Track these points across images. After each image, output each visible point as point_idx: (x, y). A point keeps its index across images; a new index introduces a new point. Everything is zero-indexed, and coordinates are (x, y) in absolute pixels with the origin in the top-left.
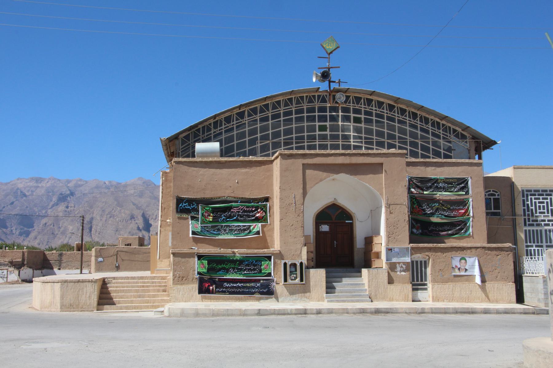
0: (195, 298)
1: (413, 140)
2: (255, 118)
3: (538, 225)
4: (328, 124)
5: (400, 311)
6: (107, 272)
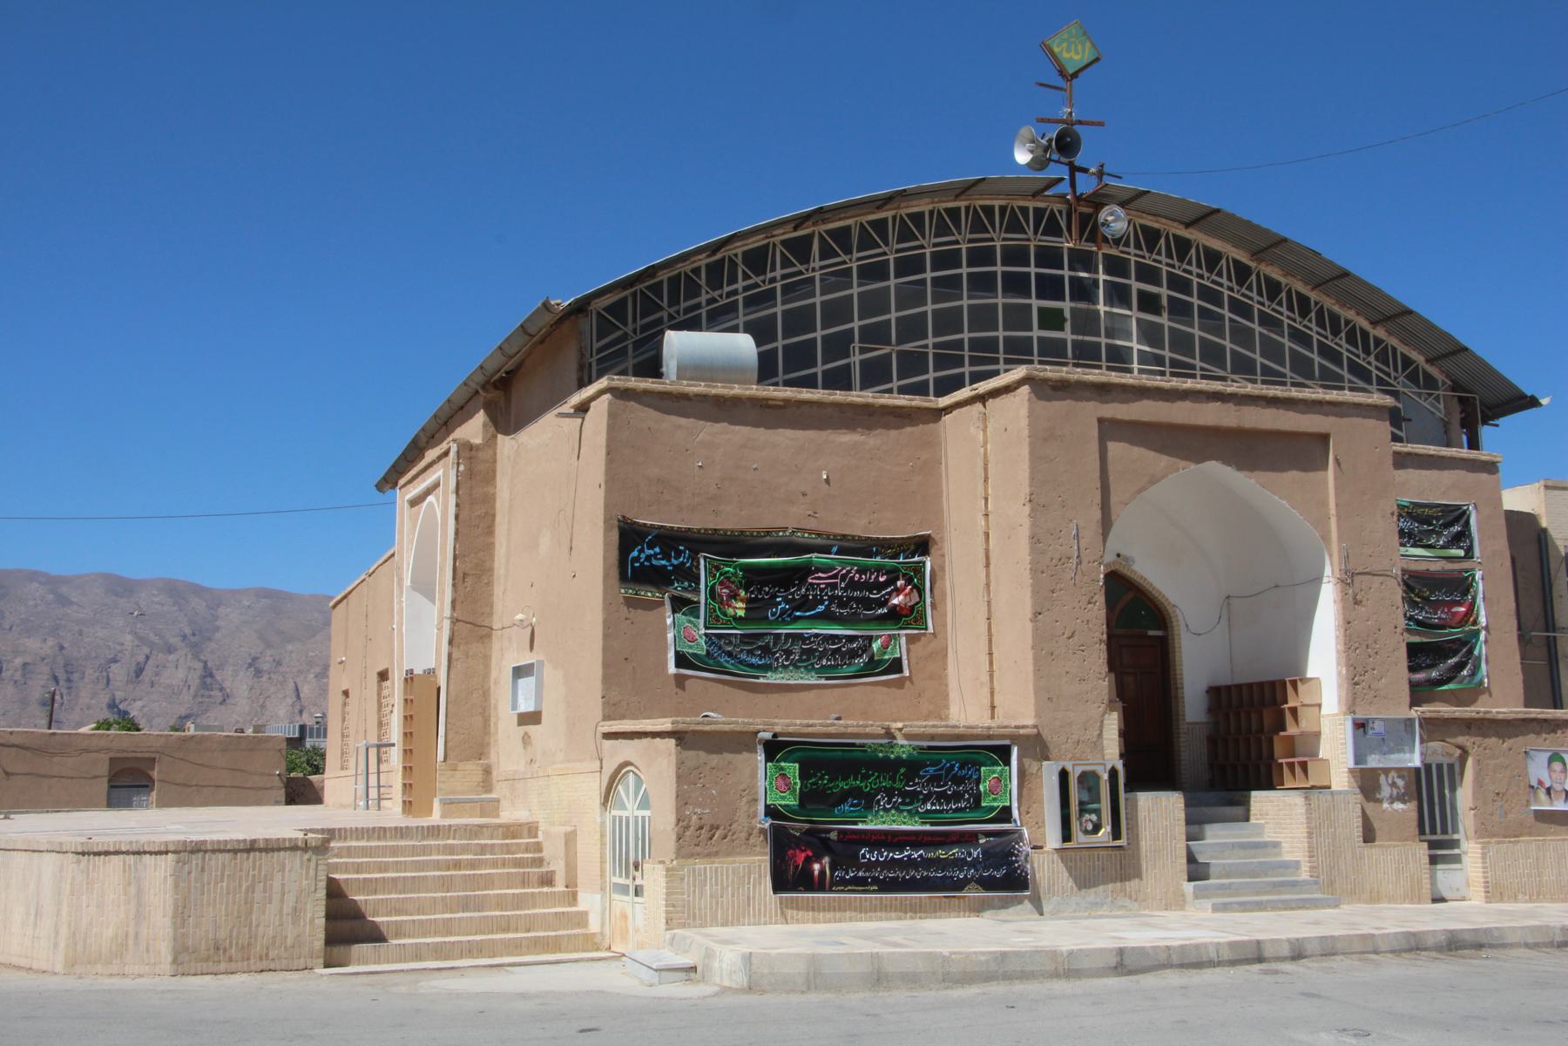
0: (760, 910)
2: (844, 262)
4: (1066, 306)
5: (1509, 941)
6: (27, 812)
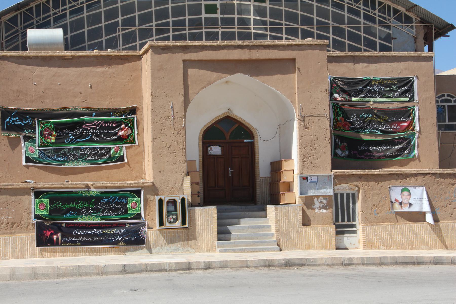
0: (32, 253)
1: (337, 25)
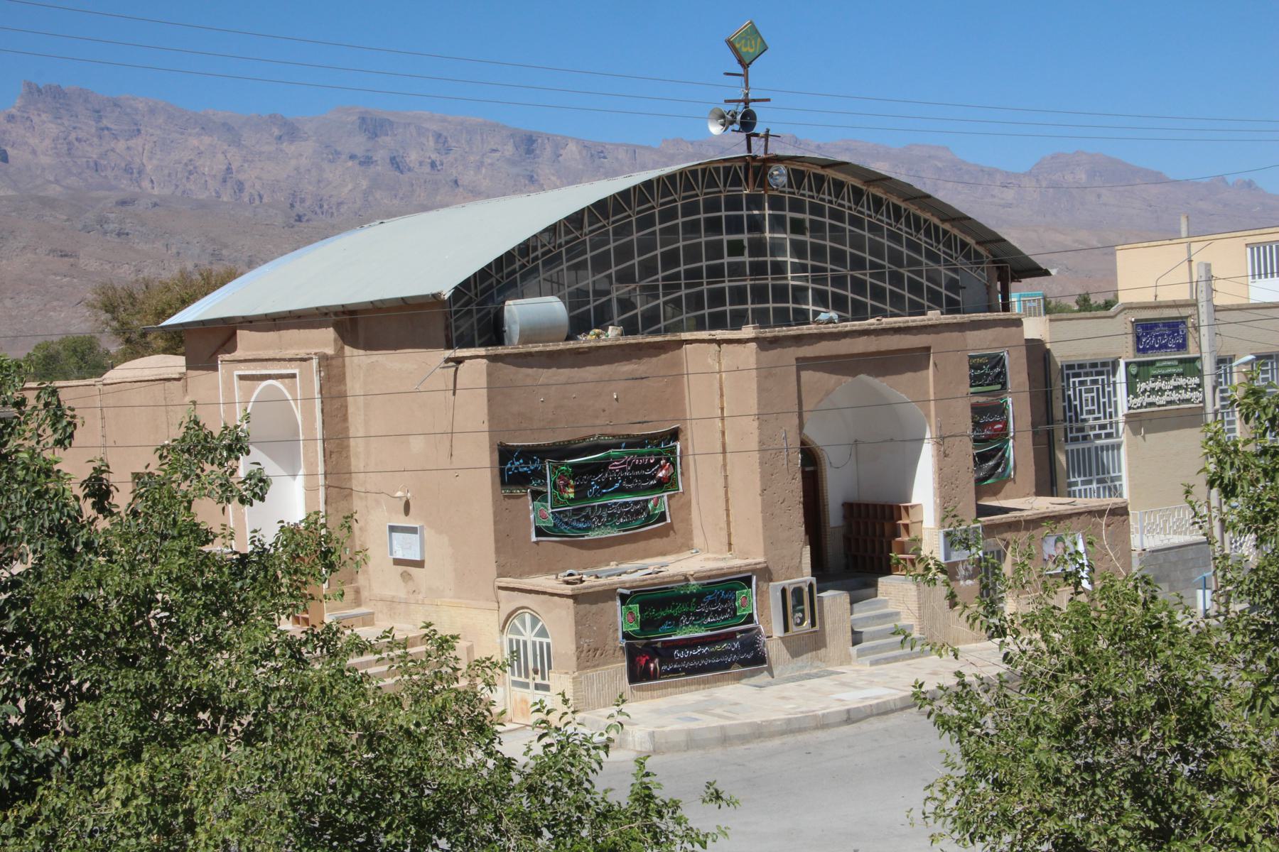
1: (894, 268)
3: (1085, 438)
